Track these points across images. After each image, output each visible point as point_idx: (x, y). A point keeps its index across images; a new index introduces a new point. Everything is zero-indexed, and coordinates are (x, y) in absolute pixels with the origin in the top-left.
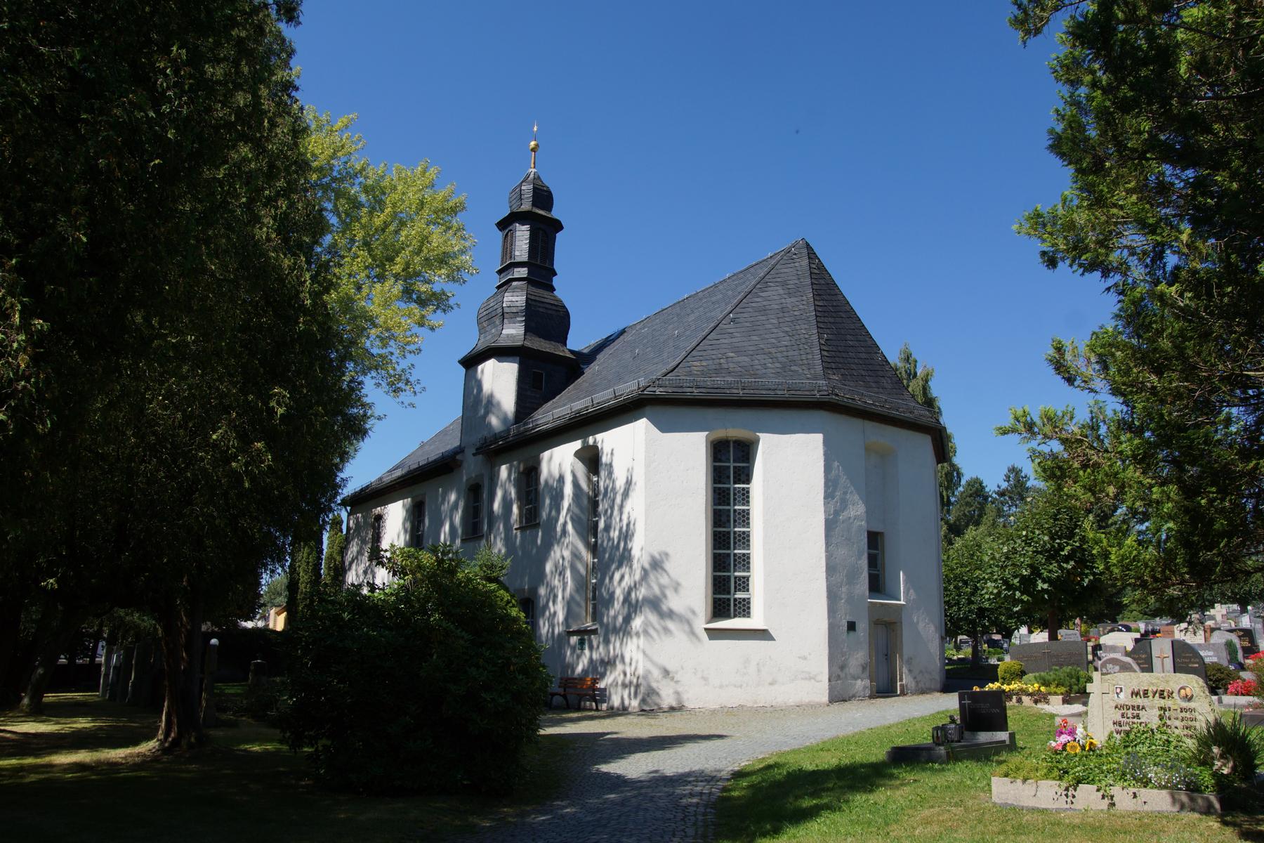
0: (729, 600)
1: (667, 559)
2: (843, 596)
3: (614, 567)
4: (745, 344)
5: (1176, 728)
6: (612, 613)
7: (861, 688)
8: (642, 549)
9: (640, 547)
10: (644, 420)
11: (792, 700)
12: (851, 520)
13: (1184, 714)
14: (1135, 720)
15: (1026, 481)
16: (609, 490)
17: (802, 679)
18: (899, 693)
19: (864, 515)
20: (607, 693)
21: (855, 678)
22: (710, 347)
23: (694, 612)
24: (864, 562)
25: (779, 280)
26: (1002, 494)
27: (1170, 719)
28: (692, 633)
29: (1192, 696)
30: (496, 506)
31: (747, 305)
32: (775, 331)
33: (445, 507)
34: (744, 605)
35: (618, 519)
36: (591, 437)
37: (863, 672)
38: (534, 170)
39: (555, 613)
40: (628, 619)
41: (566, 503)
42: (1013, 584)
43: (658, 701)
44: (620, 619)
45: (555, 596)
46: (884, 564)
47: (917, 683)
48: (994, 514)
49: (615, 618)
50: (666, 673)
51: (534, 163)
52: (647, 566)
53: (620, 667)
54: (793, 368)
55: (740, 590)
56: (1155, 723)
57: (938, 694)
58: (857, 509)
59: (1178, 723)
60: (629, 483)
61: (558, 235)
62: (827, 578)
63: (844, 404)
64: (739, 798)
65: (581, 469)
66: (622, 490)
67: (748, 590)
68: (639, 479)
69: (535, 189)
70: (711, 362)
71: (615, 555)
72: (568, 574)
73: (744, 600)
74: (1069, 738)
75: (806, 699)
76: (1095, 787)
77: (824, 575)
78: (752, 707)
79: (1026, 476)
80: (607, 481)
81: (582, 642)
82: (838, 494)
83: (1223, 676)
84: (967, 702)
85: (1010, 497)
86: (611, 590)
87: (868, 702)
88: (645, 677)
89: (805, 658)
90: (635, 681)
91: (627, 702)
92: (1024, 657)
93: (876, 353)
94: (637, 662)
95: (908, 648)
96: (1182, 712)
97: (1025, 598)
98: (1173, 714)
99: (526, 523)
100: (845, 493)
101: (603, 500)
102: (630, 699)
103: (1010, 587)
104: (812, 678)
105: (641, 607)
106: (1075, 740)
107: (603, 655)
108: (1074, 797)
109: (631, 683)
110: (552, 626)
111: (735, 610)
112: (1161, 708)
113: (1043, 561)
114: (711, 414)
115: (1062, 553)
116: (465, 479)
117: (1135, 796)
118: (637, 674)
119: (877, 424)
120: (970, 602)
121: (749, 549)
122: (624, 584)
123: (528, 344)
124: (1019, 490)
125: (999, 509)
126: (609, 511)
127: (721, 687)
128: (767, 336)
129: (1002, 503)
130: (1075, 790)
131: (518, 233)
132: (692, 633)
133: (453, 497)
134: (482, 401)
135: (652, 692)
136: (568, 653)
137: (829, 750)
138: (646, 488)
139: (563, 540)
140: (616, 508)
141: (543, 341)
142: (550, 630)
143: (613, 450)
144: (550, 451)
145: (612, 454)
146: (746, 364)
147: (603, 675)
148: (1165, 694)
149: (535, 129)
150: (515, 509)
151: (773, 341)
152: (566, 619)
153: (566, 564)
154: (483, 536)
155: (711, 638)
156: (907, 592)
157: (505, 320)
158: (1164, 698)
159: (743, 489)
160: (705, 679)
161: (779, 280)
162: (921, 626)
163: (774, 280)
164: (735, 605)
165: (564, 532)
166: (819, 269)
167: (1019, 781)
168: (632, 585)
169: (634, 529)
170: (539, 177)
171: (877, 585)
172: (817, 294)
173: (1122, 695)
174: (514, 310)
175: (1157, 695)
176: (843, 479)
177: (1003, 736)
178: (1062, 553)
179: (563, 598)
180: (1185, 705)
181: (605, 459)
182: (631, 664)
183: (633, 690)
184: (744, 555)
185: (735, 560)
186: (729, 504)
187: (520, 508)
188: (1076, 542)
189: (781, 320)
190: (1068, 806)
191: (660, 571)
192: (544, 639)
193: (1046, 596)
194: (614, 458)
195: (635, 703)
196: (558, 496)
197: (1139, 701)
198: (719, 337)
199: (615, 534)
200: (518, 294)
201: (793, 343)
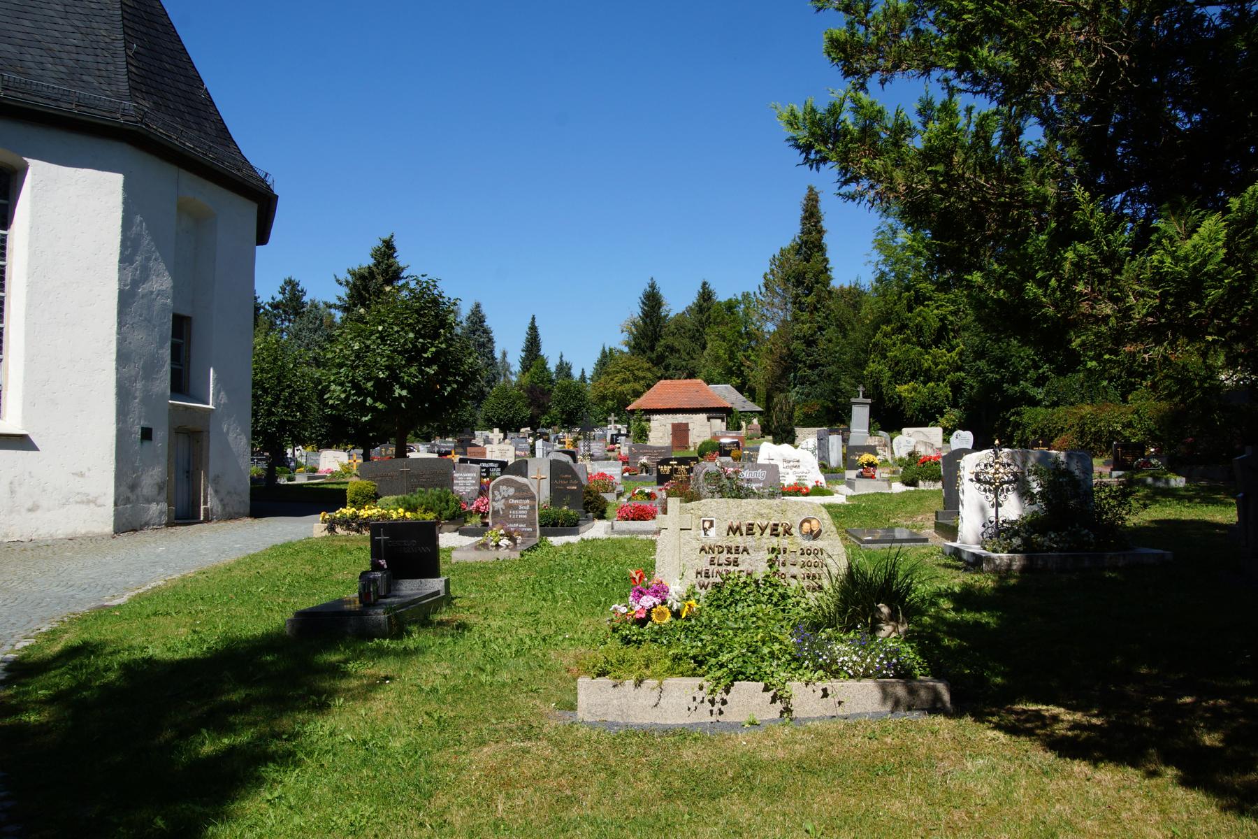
2: (138, 394)
4: (9, 27)
5: (794, 577)
11: (62, 530)
12: (154, 296)
13: (805, 558)
14: (731, 568)
15: (303, 295)
17: (77, 502)
18: (202, 518)
19: (170, 291)
21: (149, 501)
24: (166, 353)
26: (275, 306)
27: (784, 564)
29: (820, 531)
32: (61, 21)
37: (159, 494)
42: (366, 389)
46: (189, 356)
47: (224, 506)
48: (267, 326)
54: (85, 78)
56: (761, 570)
57: (249, 520)
58: (161, 283)
59: (795, 570)
62: (117, 369)
64: (41, 728)
74: (657, 601)
75: (82, 530)
76: (761, 685)
79: (302, 291)
83: (592, 499)
84: (383, 538)
85: (284, 311)
87: (166, 532)
89: (82, 475)
92: (377, 476)
93: (199, 88)
95: (215, 464)
96: (802, 554)
97: (380, 406)
98: (789, 557)
100: (148, 259)
103: (360, 390)
104: (90, 501)
106: (664, 603)
108: (724, 702)
112: (773, 550)
113: (403, 362)
115: (425, 355)
117: (825, 694)
119: (196, 176)
120: (270, 413)
124: (295, 304)
125: (271, 322)
128: (46, 25)
129: (275, 316)
130: (727, 691)
137: (168, 614)
146: (9, 56)
148: (780, 529)
151: (56, 34)
158: (777, 535)
162: (231, 436)
167: (630, 683)
171: (181, 383)
173: (712, 532)
175: (768, 531)
176: (147, 240)
177: (436, 584)
178: (425, 355)
180: (807, 544)
188: (441, 343)
189: (68, 9)
190: (713, 719)
193: (403, 405)
197: (738, 540)
201: (87, 44)
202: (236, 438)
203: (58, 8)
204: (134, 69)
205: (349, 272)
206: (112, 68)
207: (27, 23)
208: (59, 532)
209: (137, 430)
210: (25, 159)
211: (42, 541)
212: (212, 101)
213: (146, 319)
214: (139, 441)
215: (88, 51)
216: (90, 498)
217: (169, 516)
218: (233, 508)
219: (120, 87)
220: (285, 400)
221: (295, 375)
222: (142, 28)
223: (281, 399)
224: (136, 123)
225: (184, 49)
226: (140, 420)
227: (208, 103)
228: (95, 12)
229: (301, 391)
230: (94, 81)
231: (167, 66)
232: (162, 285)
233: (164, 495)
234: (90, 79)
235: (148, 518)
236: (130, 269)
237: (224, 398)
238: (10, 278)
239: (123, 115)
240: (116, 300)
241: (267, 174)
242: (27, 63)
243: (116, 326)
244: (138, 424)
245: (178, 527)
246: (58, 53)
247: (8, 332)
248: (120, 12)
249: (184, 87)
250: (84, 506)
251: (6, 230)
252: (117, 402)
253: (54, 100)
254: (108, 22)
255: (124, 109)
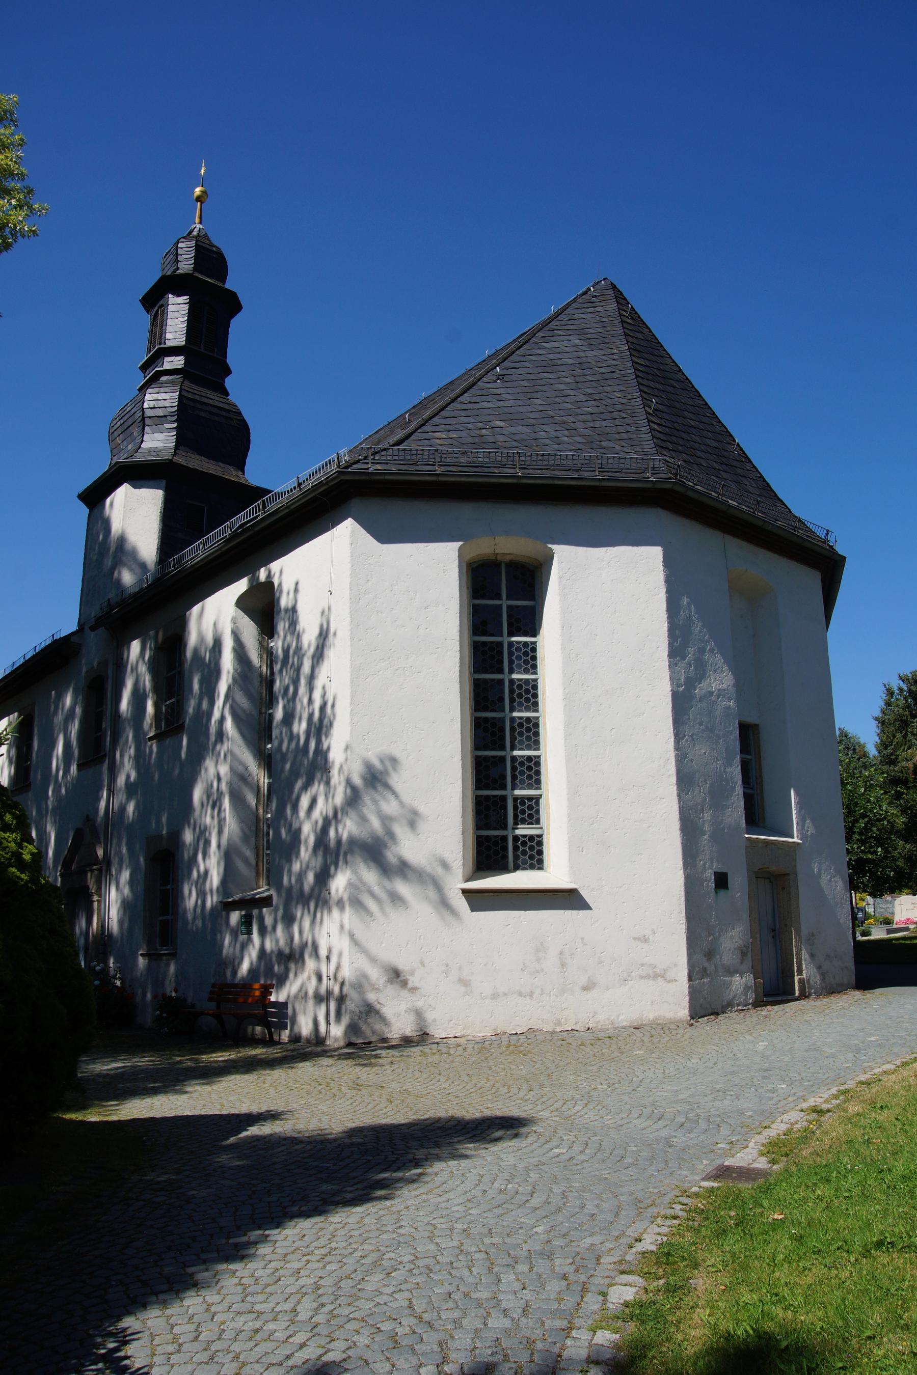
0: (505, 839)
1: (395, 769)
2: (706, 827)
3: (299, 784)
4: (521, 409)
6: (296, 867)
7: (741, 989)
8: (347, 748)
9: (343, 746)
10: (350, 519)
11: (625, 1016)
12: (713, 698)
16: (291, 652)
17: (642, 977)
19: (732, 690)
20: (290, 1011)
21: (731, 972)
22: (463, 413)
23: (445, 865)
24: (736, 771)
25: (572, 327)
28: (444, 903)
30: (124, 705)
31: (522, 359)
32: (572, 393)
33: (60, 718)
34: (532, 848)
35: (305, 701)
36: (263, 570)
37: (742, 963)
38: (199, 226)
39: (206, 872)
40: (323, 877)
41: (223, 687)
43: (378, 1026)
44: (310, 878)
45: (207, 843)
46: (761, 776)
47: (823, 975)
49: (301, 876)
50: (396, 976)
51: (200, 217)
52: (357, 780)
53: (310, 964)
54: (604, 444)
55: (523, 821)
57: (858, 994)
60: (324, 635)
61: (234, 322)
62: (679, 795)
63: (696, 496)
65: (250, 630)
66: (312, 649)
67: (538, 821)
68: (341, 625)
69: (198, 248)
70: (464, 434)
71: (301, 764)
72: (226, 803)
73: (531, 838)
75: (650, 1015)
77: (674, 790)
78: (552, 1033)
80: (289, 638)
81: (247, 922)
82: (691, 650)
86: (295, 825)
88: (358, 986)
89: (645, 940)
90: (336, 989)
91: (323, 1028)
94: (340, 955)
99: (167, 725)
100: (702, 651)
101: (281, 671)
102: (328, 1022)
105: (346, 854)
107: (282, 943)
109: (329, 993)
110: (202, 894)
111: (516, 857)
114: (466, 511)
116: (84, 670)
118: (340, 979)
121: (538, 749)
122: (317, 814)
123: (179, 460)
126: (291, 689)
127: (495, 996)
128: (557, 400)
131: (171, 308)
132: (444, 903)
133: (68, 700)
134: (109, 549)
135: (370, 1010)
136: (227, 940)
138: (352, 639)
139: (218, 747)
140: (303, 681)
141: (206, 460)
142: (199, 902)
143: (297, 584)
144: (200, 604)
145: (296, 590)
147: (282, 980)
149: (203, 171)
150: (150, 708)
151: (569, 406)
152: (224, 882)
153: (224, 787)
154: (105, 755)
155: (474, 907)
156: (802, 823)
157: (147, 429)
159: (526, 644)
160: (464, 983)
161: (572, 327)
162: (825, 878)
163: (566, 327)
164: (516, 848)
165: (221, 735)
166: (632, 318)
168: (331, 814)
169: (334, 715)
170: (206, 236)
172: (635, 350)
174: (160, 412)
176: (697, 627)
179: (219, 846)
181: (285, 602)
182: (328, 958)
183: (333, 1006)
184: (529, 758)
185: (514, 769)
186: (501, 671)
187: (157, 705)
191: (380, 788)
192: (190, 916)
194: (300, 597)
195: (337, 1031)
196: (212, 673)
198: (478, 399)
199: (300, 727)
200: (167, 389)
201: (601, 409)
202: (830, 880)
203: (568, 380)
204: (656, 427)
205: (901, 678)
206: (633, 429)
207: (538, 402)
208: (621, 1017)
209: (710, 875)
210: (550, 546)
211: (601, 1030)
212: (747, 457)
213: (707, 727)
214: (713, 890)
215: (604, 416)
216: (657, 970)
217: (756, 992)
218: (834, 978)
219: (645, 447)
220: (860, 834)
221: (869, 801)
222: (658, 386)
223: (854, 833)
224: (670, 478)
225: (706, 404)
226: (712, 863)
227: (743, 460)
228: (606, 376)
229: (879, 820)
230: (614, 445)
231: (691, 422)
232: (721, 683)
233: (748, 963)
234: (610, 444)
235: (731, 996)
236: (682, 664)
237: (811, 830)
238: (544, 694)
239: (653, 474)
240: (670, 706)
241: (828, 532)
242: (542, 441)
243: (673, 739)
244: (710, 868)
245: (769, 1008)
246: (572, 425)
247: (546, 760)
248: (633, 371)
249: (713, 443)
250: (651, 982)
251: (535, 636)
252: (683, 839)
253: (574, 470)
254: (621, 382)
255: (654, 468)
